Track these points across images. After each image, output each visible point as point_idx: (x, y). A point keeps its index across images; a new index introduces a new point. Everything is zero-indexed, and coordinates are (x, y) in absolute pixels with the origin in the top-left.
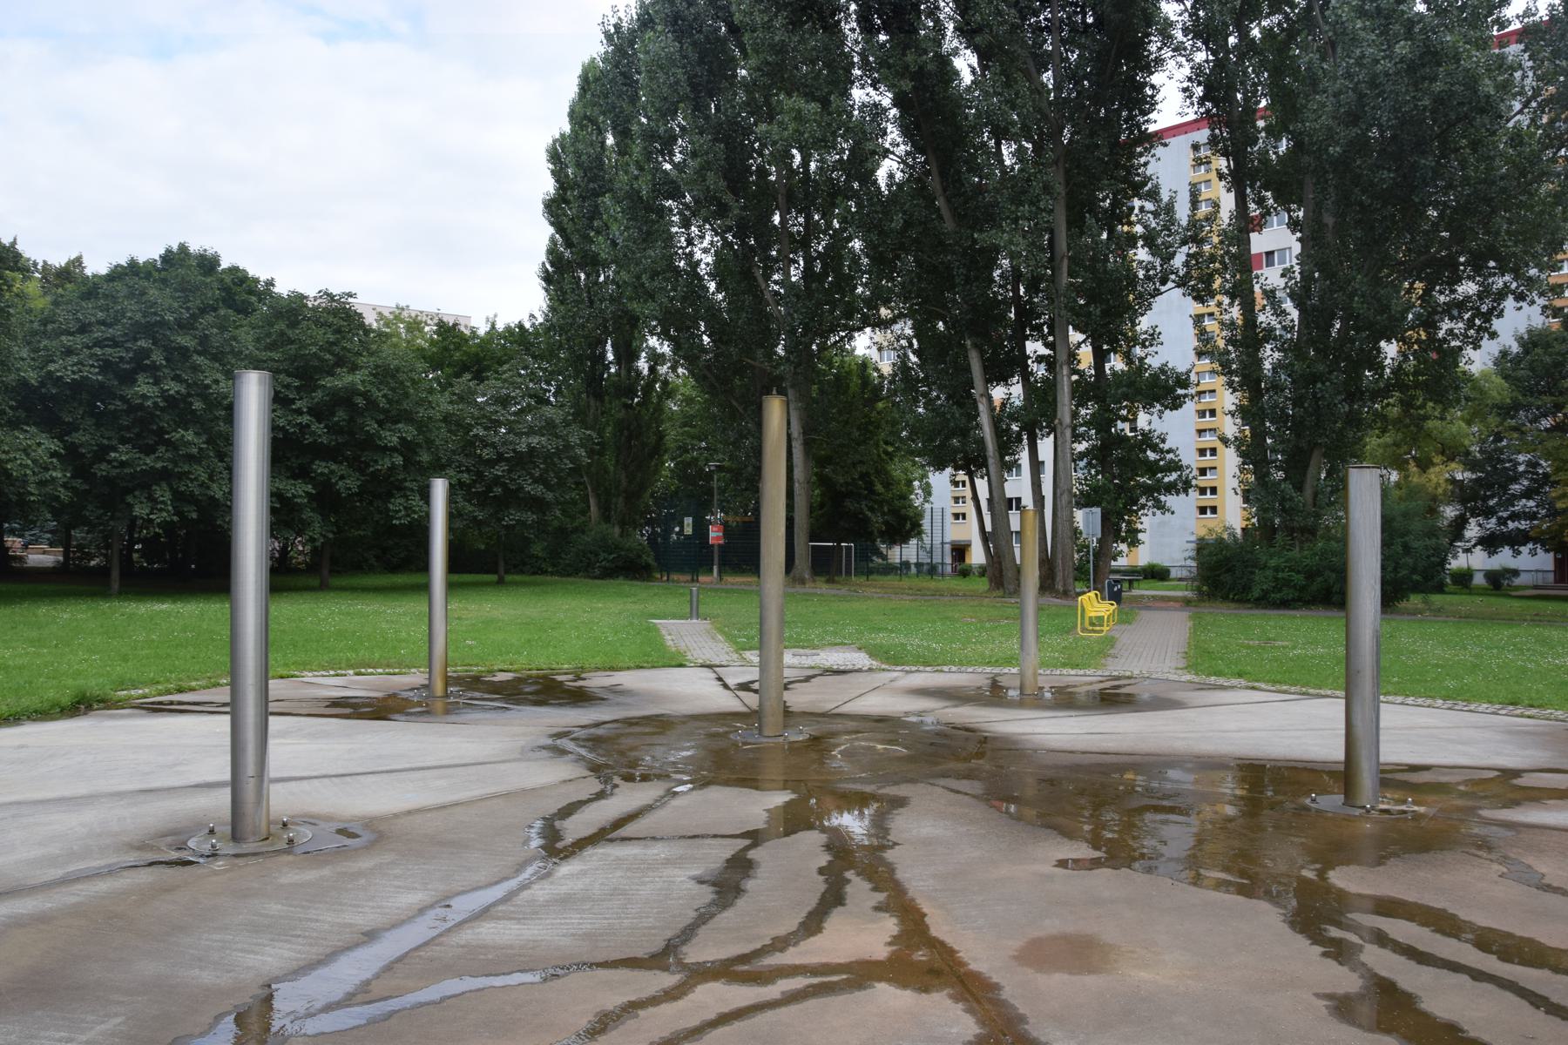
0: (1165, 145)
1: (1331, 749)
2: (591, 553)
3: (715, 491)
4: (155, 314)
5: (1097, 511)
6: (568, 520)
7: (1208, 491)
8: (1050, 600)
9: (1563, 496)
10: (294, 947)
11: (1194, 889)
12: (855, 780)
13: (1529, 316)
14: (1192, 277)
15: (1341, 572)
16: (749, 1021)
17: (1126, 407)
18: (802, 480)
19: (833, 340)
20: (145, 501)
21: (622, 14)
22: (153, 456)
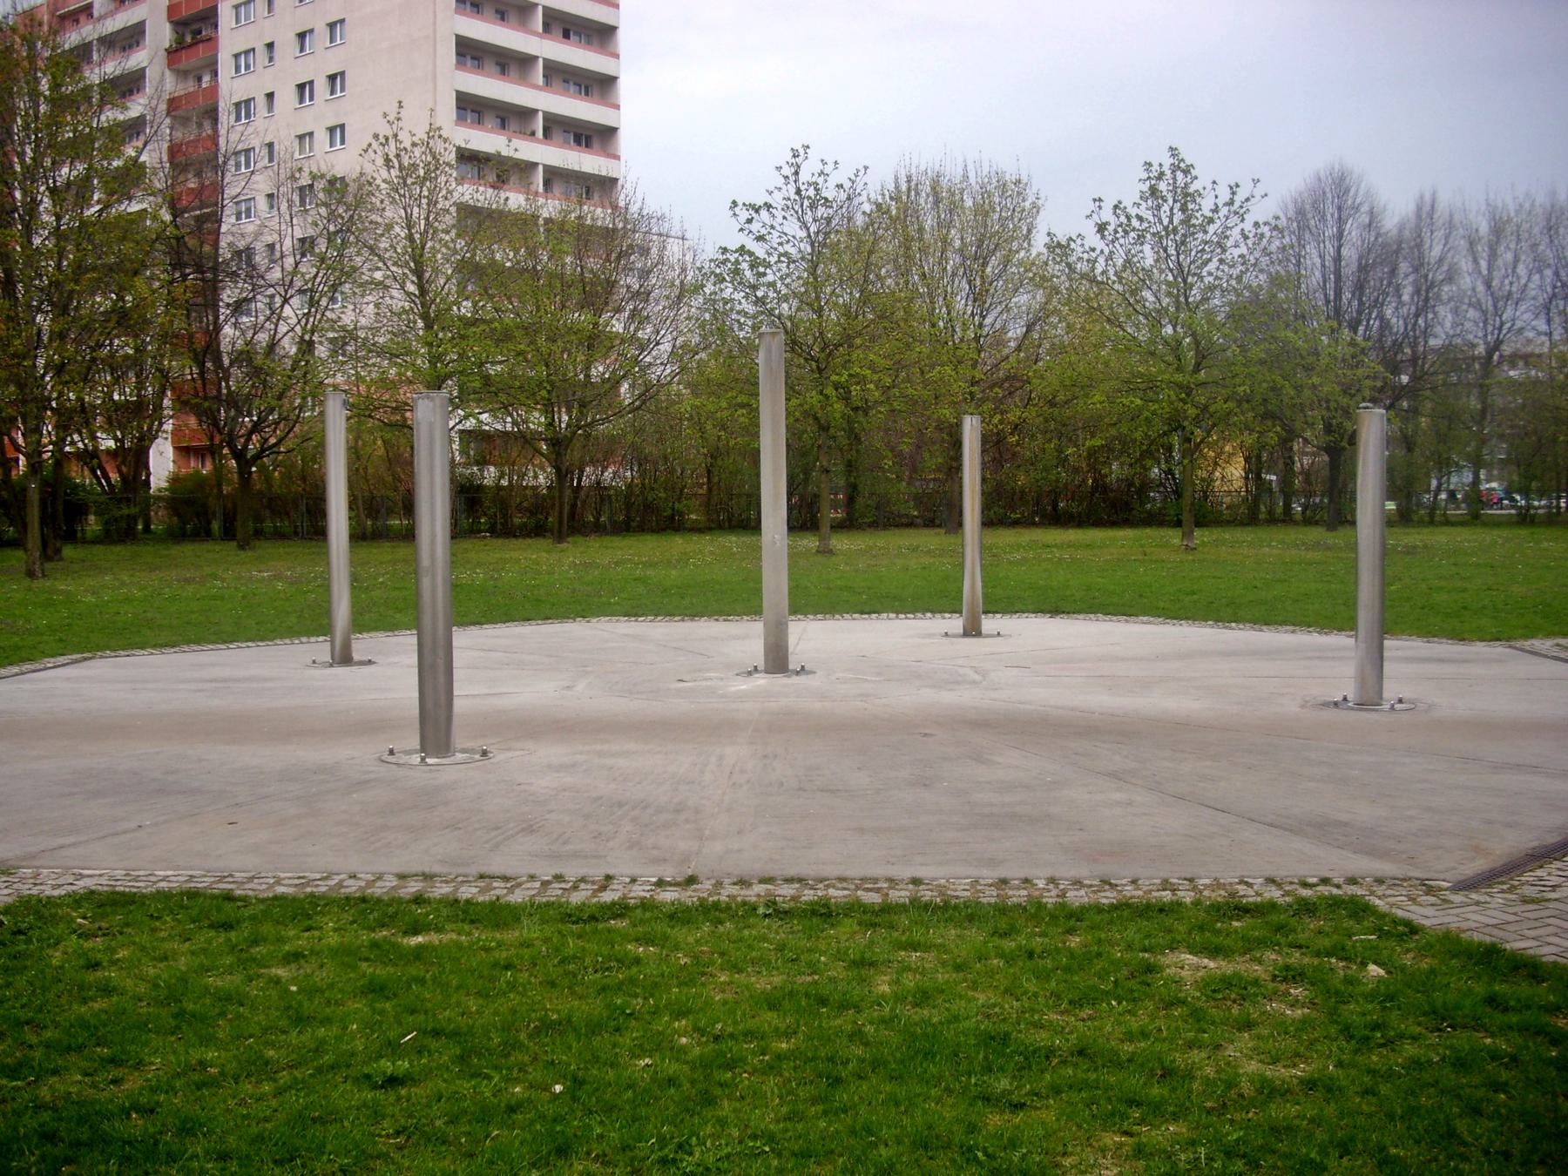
0: (1036, 208)
1: (468, 643)
2: (974, 682)
3: (34, 515)
4: (936, 243)
5: (454, 628)
6: (635, 969)
7: (539, 178)
8: (810, 542)
9: (867, 1173)
10: (1514, 1019)
11: (1359, 523)
12: (561, 513)
13: (400, 102)
14: (850, 375)
15: (1351, 603)
16: (608, 626)
17: (604, 374)
18: (603, 900)
19: (1518, 498)
20: (1297, 1122)
21: (913, 171)
22: (959, 932)
